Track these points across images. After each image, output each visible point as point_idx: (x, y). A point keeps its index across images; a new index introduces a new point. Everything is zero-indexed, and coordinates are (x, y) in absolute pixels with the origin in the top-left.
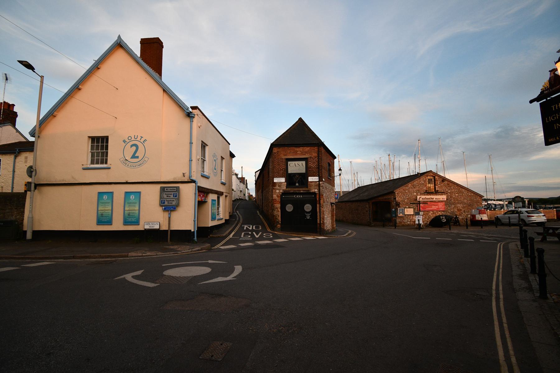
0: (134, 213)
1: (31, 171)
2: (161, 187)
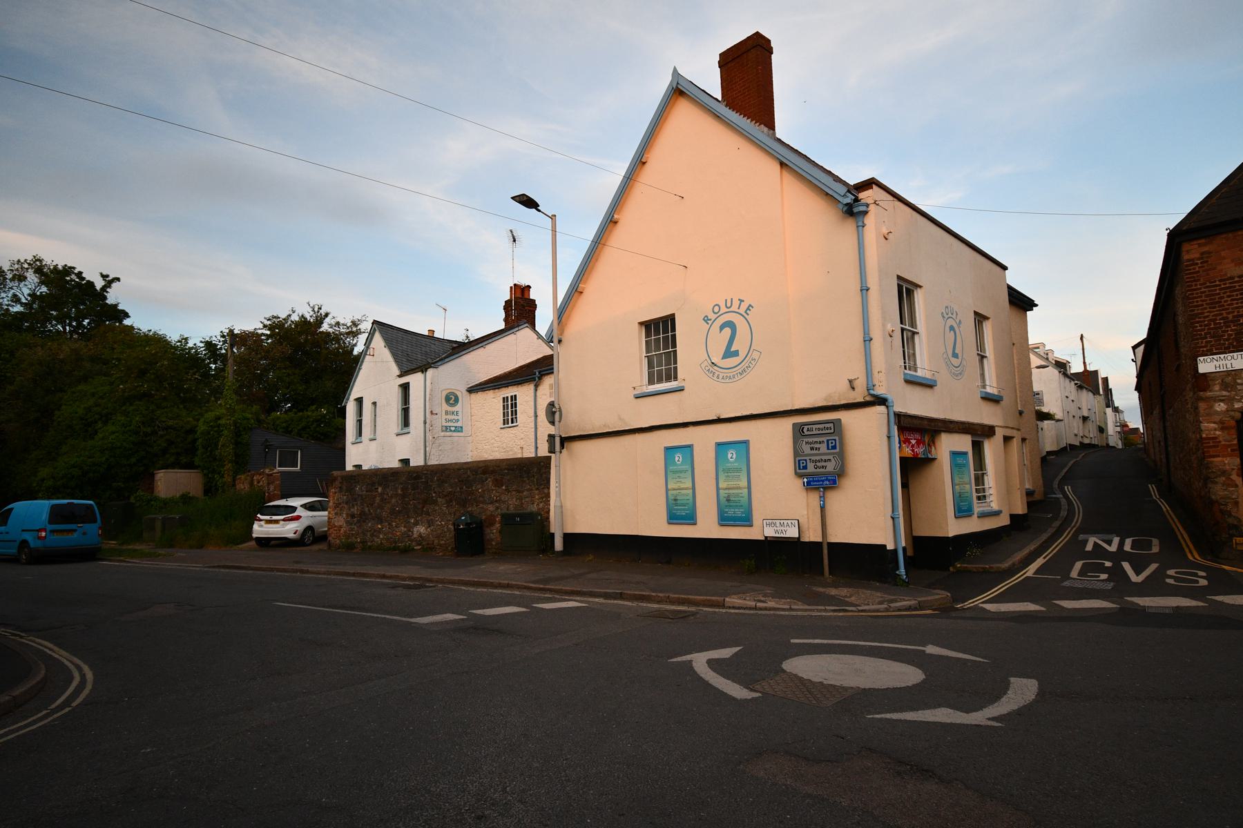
0: (737, 495)
1: (553, 412)
2: (794, 424)
